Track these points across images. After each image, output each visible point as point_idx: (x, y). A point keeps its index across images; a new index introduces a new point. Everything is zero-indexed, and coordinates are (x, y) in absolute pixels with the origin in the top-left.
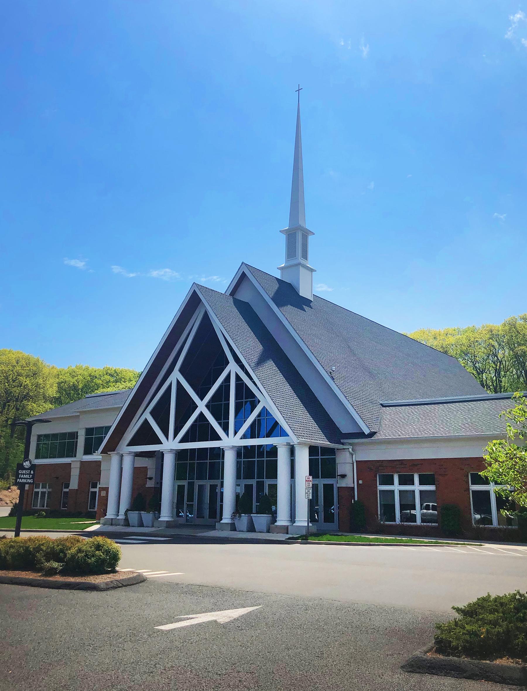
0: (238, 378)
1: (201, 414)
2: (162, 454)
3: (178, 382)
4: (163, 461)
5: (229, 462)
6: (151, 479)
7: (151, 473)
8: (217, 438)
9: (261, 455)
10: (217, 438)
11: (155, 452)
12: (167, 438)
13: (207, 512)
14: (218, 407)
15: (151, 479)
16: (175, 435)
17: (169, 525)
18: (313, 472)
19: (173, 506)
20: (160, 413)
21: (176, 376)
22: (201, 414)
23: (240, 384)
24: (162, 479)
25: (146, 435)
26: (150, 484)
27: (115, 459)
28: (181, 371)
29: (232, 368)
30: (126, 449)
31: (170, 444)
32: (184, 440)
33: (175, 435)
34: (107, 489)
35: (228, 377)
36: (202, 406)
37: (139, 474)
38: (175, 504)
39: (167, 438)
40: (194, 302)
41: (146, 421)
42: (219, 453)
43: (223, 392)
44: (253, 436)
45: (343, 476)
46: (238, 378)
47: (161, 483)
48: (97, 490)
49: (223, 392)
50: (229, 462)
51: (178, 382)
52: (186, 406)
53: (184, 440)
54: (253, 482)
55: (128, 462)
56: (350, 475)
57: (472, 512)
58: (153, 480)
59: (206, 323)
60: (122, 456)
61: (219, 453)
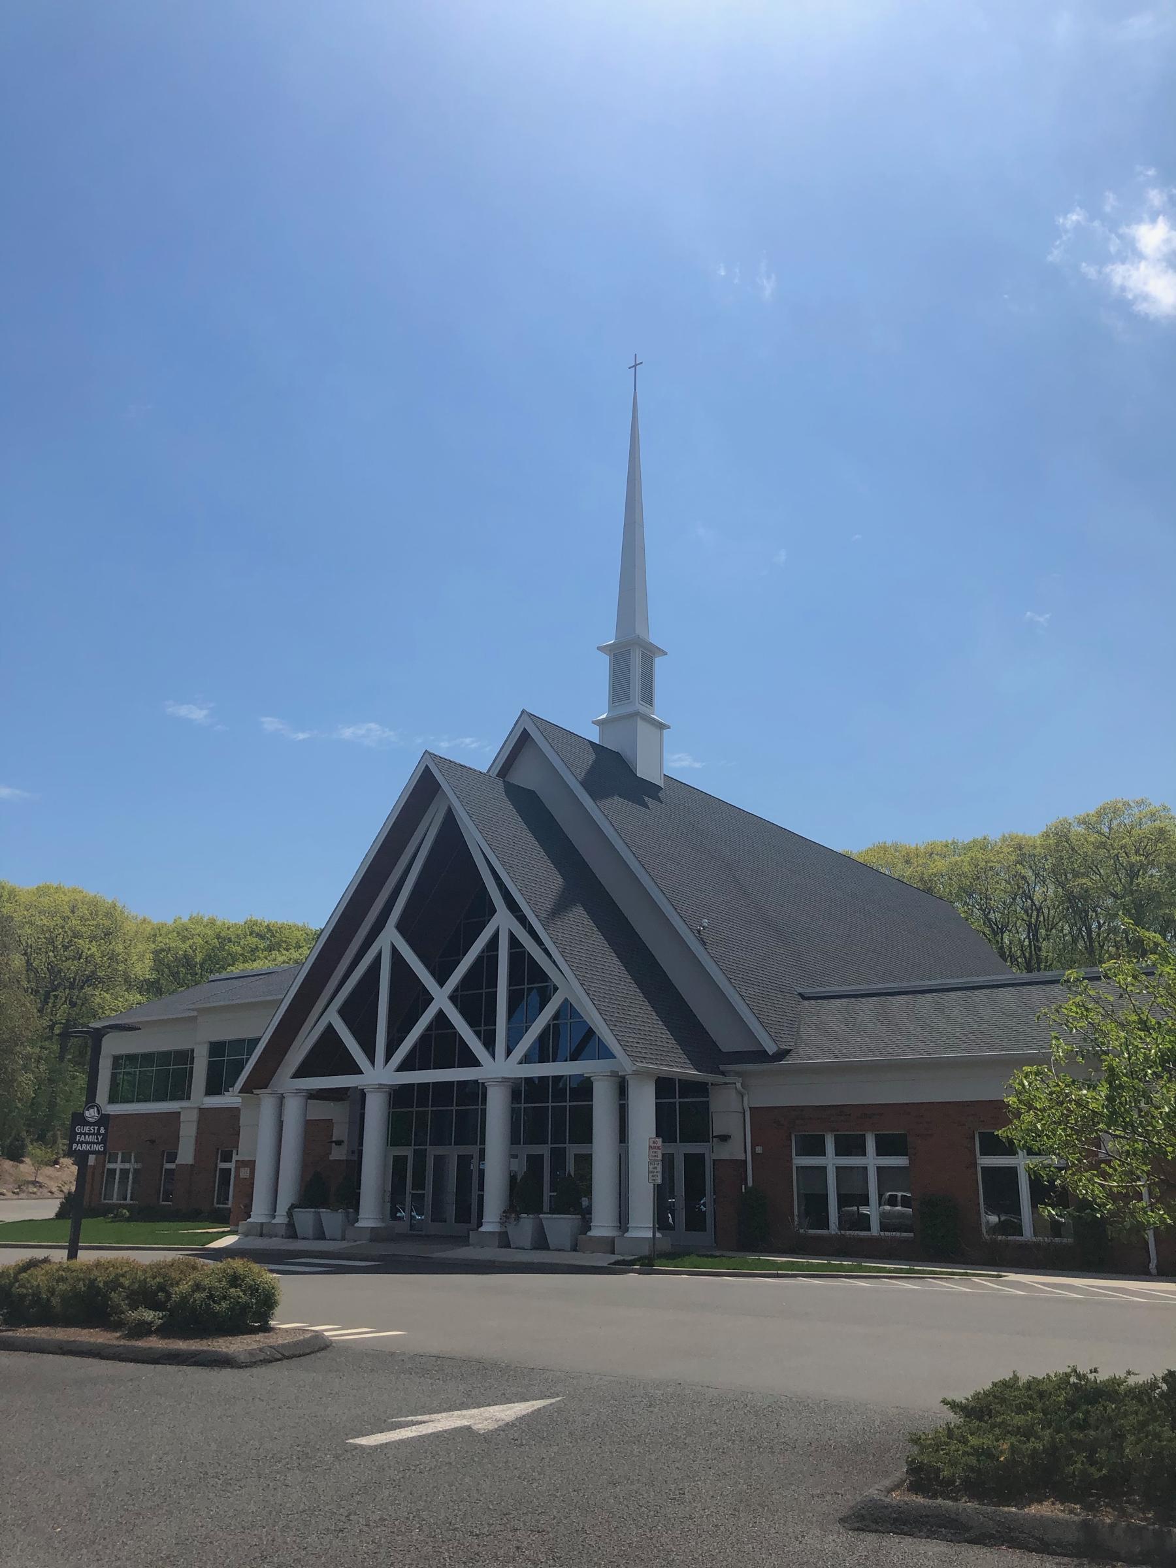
0: (514, 941)
1: (441, 1015)
2: (363, 1094)
3: (394, 950)
4: (363, 1107)
6: (339, 1143)
7: (340, 1132)
12: (373, 1063)
13: (451, 1210)
14: (475, 1001)
15: (339, 1143)
16: (388, 1057)
21: (390, 937)
22: (441, 1015)
24: (361, 1144)
25: (329, 1057)
27: (267, 1104)
28: (400, 927)
29: (502, 921)
31: (378, 1075)
32: (404, 1067)
33: (388, 1057)
34: (251, 1165)
35: (495, 938)
36: (441, 999)
37: (316, 1134)
38: (388, 1194)
39: (373, 1063)
40: (425, 788)
41: (330, 1028)
44: (425, 1067)
45: (725, 1138)
51: (394, 950)
53: (404, 1067)
54: (545, 1150)
57: (982, 1210)
60: (282, 1098)
61: (475, 1093)
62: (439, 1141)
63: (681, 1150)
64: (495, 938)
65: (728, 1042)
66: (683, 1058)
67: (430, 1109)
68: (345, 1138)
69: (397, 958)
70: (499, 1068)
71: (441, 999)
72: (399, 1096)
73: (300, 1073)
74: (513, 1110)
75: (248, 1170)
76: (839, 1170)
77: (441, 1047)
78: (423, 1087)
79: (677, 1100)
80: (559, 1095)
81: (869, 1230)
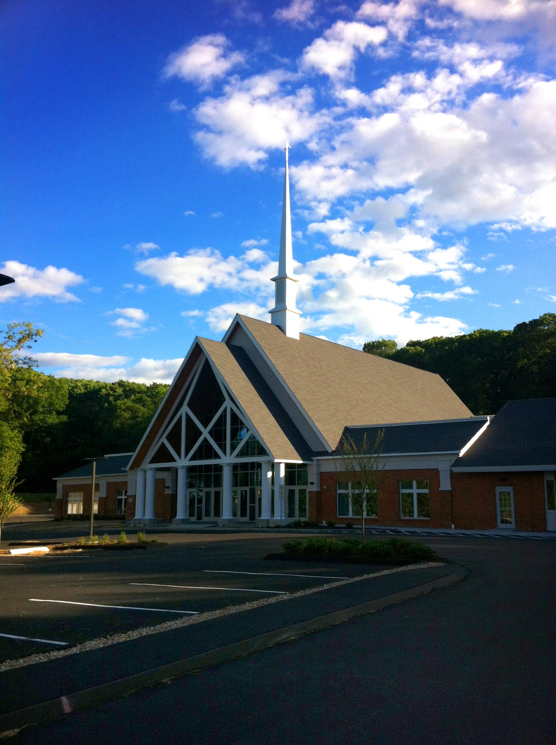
0: (232, 410)
1: (205, 440)
2: (177, 469)
3: (187, 415)
4: (177, 474)
5: (227, 476)
6: (168, 488)
7: (168, 483)
8: (217, 456)
9: (201, 471)
10: (217, 456)
11: (170, 468)
12: (180, 457)
13: (212, 512)
14: (218, 434)
15: (168, 488)
16: (186, 454)
17: (183, 521)
18: (235, 483)
19: (186, 508)
20: (174, 438)
21: (185, 409)
22: (205, 440)
23: (234, 417)
24: (177, 487)
25: (163, 455)
26: (168, 492)
27: (140, 474)
28: (189, 405)
29: (228, 404)
30: (148, 466)
31: (182, 462)
32: (193, 458)
33: (186, 454)
34: (134, 497)
35: (225, 410)
36: (205, 433)
37: (159, 484)
38: (188, 507)
39: (180, 457)
40: (197, 352)
41: (163, 444)
42: (219, 468)
43: (222, 421)
44: (201, 458)
45: (312, 483)
46: (232, 410)
47: (177, 491)
48: (123, 497)
49: (222, 421)
50: (227, 476)
51: (187, 415)
52: (193, 434)
53: (193, 458)
54: (247, 489)
55: (150, 476)
56: (316, 482)
57: (547, 508)
58: (315, 485)
59: (208, 368)
60: (145, 471)
61: (219, 468)
62: (208, 485)
63: (239, 489)
64: (225, 410)
65: (315, 449)
66: (296, 454)
67: (296, 470)
68: (171, 486)
69: (188, 418)
70: (227, 460)
71: (205, 433)
72: (191, 470)
73: (152, 462)
74: (233, 474)
75: (132, 499)
76: (418, 494)
77: (206, 451)
78: (201, 466)
79: (213, 473)
80: (201, 471)
81: (413, 516)
